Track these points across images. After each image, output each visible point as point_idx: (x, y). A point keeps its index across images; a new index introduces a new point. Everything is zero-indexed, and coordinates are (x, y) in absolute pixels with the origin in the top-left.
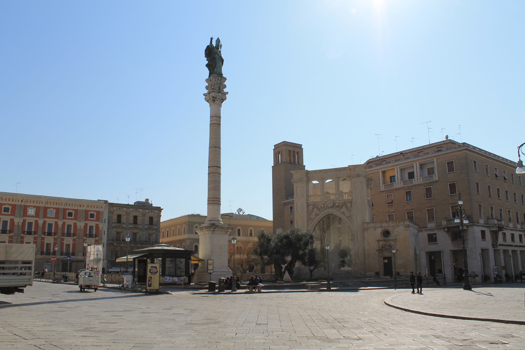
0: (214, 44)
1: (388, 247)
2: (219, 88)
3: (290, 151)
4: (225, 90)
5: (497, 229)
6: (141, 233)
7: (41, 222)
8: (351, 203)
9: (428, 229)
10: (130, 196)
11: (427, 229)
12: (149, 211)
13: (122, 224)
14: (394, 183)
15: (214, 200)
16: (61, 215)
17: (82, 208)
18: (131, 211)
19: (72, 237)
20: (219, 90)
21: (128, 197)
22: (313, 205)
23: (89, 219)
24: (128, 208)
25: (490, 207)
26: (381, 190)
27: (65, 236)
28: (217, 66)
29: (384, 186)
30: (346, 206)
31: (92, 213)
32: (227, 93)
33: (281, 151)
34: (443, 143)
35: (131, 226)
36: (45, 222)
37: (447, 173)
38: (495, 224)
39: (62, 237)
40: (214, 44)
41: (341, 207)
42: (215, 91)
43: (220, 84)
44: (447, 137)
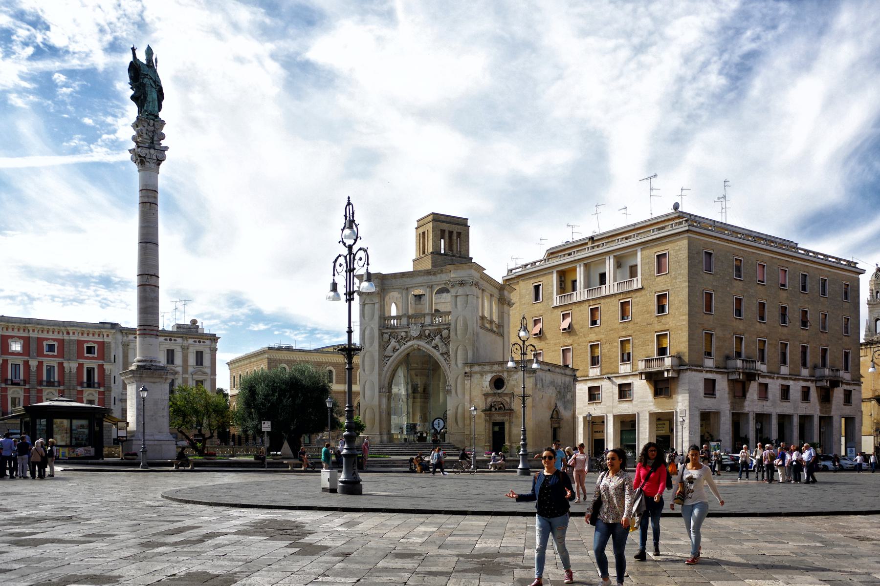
0: (142, 57)
1: (500, 406)
2: (152, 139)
3: (444, 231)
4: (164, 143)
5: (741, 378)
7: (33, 363)
8: (449, 331)
9: (620, 375)
10: (165, 314)
11: (618, 375)
15: (145, 329)
16: (33, 346)
17: (73, 337)
19: (56, 387)
20: (152, 143)
23: (86, 355)
25: (736, 337)
26: (555, 305)
27: (44, 386)
28: (148, 99)
30: (441, 335)
31: (52, 343)
32: (166, 148)
34: (667, 218)
36: (40, 364)
38: (737, 368)
39: (39, 388)
40: (142, 57)
42: (143, 145)
43: (154, 131)
44: (676, 207)
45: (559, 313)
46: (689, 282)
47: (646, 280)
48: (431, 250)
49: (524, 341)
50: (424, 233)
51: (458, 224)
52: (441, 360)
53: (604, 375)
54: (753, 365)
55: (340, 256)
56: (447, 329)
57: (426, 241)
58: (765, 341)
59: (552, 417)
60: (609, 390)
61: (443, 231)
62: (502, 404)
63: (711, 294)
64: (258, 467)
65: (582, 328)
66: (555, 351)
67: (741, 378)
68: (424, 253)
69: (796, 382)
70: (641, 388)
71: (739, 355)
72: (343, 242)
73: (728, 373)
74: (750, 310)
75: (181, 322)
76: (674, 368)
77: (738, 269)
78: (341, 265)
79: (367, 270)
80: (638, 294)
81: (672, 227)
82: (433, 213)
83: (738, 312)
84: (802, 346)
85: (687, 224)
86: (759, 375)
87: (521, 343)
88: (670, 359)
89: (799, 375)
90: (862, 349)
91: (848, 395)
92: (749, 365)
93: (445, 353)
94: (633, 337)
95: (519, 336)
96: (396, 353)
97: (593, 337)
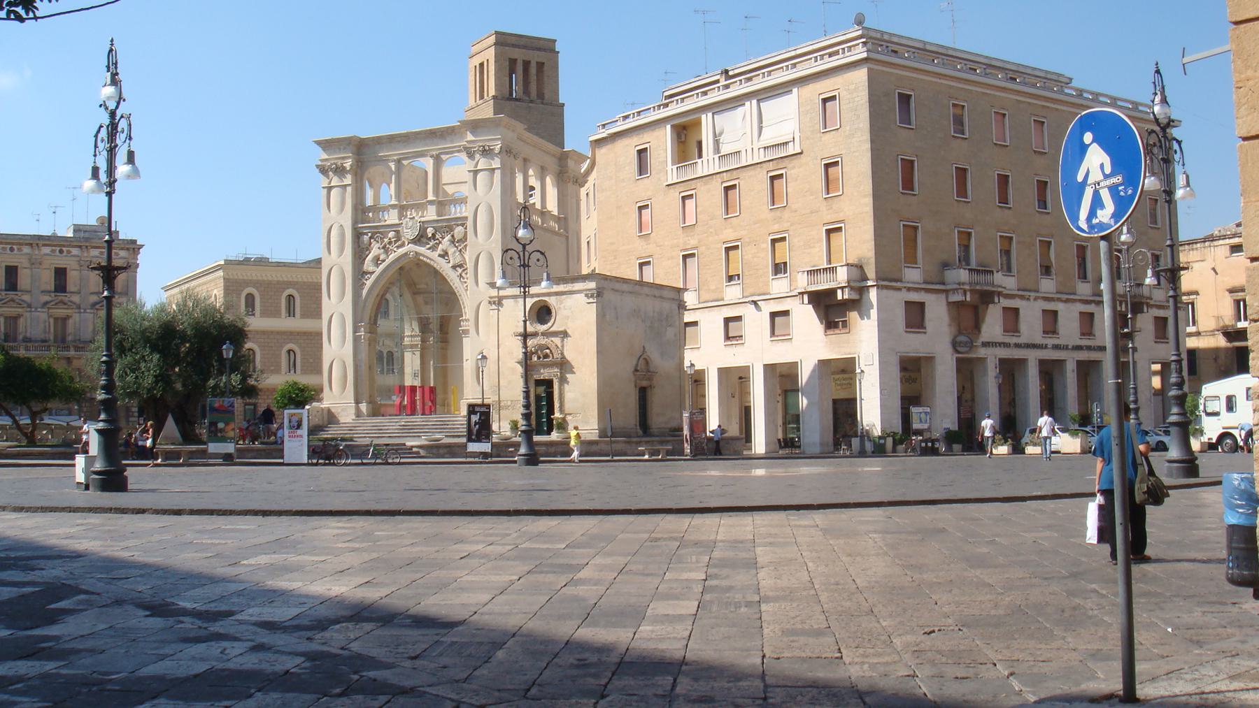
5: (968, 299)
6: (76, 317)
8: (466, 228)
12: (53, 251)
13: (19, 293)
14: (700, 161)
18: (47, 255)
21: (54, 212)
22: (370, 234)
24: (37, 244)
25: (958, 232)
29: (675, 170)
33: (488, 60)
35: (47, 298)
37: (822, 131)
41: (440, 239)
45: (676, 195)
46: (872, 141)
47: (807, 138)
48: (492, 92)
49: (524, 246)
50: (482, 65)
51: (539, 49)
52: (452, 276)
53: (746, 297)
54: (989, 277)
55: (101, 127)
56: (462, 225)
57: (485, 76)
58: (1011, 238)
59: (636, 370)
60: (755, 323)
61: (513, 62)
62: (548, 348)
63: (912, 162)
64: (59, 459)
65: (711, 220)
66: (672, 258)
67: (968, 299)
68: (482, 97)
69: (1069, 305)
70: (805, 318)
71: (965, 259)
72: (105, 105)
73: (946, 291)
74: (982, 186)
75: (82, 221)
76: (852, 284)
77: (959, 121)
78: (102, 141)
79: (129, 146)
80: (796, 162)
81: (844, 53)
82: (496, 33)
83: (962, 191)
84: (1077, 245)
85: (865, 49)
86: (999, 294)
87: (520, 248)
88: (845, 268)
89: (1075, 294)
90: (1182, 251)
91: (1161, 323)
92: (982, 278)
93: (458, 266)
94: (791, 233)
95: (515, 237)
96: (382, 267)
97: (729, 234)
